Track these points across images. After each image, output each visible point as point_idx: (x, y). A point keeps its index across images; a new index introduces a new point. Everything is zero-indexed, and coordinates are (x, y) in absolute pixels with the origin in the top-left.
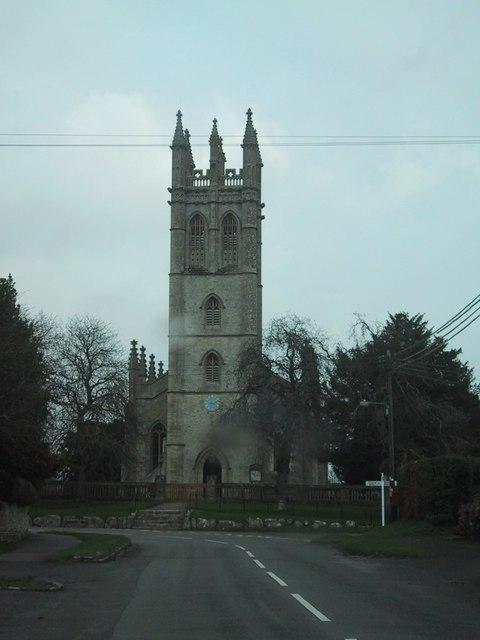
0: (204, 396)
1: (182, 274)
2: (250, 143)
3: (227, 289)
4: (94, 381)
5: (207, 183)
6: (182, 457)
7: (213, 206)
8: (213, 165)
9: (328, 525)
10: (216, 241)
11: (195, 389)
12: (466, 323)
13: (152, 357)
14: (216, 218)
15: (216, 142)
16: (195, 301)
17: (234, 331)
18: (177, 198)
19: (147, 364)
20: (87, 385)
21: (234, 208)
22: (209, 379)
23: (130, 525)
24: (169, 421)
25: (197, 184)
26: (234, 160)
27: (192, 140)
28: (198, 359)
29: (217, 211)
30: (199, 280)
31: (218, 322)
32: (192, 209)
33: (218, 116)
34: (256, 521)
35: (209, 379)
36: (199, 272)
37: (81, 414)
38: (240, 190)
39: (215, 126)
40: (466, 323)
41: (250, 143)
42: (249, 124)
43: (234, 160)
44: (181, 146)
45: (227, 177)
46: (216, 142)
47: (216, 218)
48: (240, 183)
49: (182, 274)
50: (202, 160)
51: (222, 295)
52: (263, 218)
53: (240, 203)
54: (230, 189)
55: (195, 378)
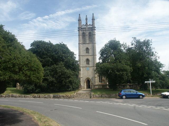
2: (93, 20)
21: (91, 31)
26: (90, 22)
38: (92, 28)
43: (90, 22)
46: (86, 19)
48: (92, 27)
50: (83, 23)
51: (89, 48)
53: (92, 30)
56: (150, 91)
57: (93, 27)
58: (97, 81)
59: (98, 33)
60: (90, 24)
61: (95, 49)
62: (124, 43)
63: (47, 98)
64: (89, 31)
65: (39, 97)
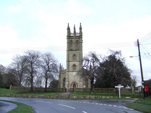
0: (73, 72)
1: (69, 50)
2: (81, 29)
3: (77, 53)
4: (49, 65)
5: (73, 35)
6: (69, 84)
7: (74, 39)
8: (74, 32)
9: (106, 97)
10: (75, 45)
11: (71, 71)
12: (149, 35)
13: (64, 68)
14: (75, 41)
15: (74, 28)
16: (71, 55)
17: (78, 61)
18: (68, 37)
19: (63, 69)
20: (48, 66)
21: (78, 39)
22: (74, 69)
23: (56, 98)
24: (66, 77)
25: (71, 35)
26: (78, 31)
27: (70, 28)
28: (72, 65)
29: (75, 40)
30: (72, 52)
31: (75, 69)
32: (70, 39)
33: (74, 25)
34: (88, 97)
35: (74, 69)
36: (72, 50)
37: (47, 72)
38: (79, 36)
39: (75, 26)
40: (144, 38)
41: (81, 29)
42: (81, 25)
43: (78, 31)
44: (69, 29)
45: (77, 34)
46: (74, 28)
47: (75, 41)
48: (79, 35)
49: (69, 50)
50: (72, 31)
51: (76, 54)
52: (83, 42)
53: (79, 38)
54: (77, 36)
55: (71, 69)
56: (120, 95)
57: (80, 36)
58: (81, 85)
59: (140, 42)
60: (78, 33)
61: (67, 58)
62: (13, 58)
63: (34, 98)
64: (76, 39)
65: (28, 97)
